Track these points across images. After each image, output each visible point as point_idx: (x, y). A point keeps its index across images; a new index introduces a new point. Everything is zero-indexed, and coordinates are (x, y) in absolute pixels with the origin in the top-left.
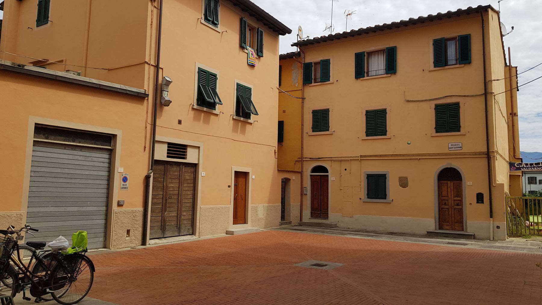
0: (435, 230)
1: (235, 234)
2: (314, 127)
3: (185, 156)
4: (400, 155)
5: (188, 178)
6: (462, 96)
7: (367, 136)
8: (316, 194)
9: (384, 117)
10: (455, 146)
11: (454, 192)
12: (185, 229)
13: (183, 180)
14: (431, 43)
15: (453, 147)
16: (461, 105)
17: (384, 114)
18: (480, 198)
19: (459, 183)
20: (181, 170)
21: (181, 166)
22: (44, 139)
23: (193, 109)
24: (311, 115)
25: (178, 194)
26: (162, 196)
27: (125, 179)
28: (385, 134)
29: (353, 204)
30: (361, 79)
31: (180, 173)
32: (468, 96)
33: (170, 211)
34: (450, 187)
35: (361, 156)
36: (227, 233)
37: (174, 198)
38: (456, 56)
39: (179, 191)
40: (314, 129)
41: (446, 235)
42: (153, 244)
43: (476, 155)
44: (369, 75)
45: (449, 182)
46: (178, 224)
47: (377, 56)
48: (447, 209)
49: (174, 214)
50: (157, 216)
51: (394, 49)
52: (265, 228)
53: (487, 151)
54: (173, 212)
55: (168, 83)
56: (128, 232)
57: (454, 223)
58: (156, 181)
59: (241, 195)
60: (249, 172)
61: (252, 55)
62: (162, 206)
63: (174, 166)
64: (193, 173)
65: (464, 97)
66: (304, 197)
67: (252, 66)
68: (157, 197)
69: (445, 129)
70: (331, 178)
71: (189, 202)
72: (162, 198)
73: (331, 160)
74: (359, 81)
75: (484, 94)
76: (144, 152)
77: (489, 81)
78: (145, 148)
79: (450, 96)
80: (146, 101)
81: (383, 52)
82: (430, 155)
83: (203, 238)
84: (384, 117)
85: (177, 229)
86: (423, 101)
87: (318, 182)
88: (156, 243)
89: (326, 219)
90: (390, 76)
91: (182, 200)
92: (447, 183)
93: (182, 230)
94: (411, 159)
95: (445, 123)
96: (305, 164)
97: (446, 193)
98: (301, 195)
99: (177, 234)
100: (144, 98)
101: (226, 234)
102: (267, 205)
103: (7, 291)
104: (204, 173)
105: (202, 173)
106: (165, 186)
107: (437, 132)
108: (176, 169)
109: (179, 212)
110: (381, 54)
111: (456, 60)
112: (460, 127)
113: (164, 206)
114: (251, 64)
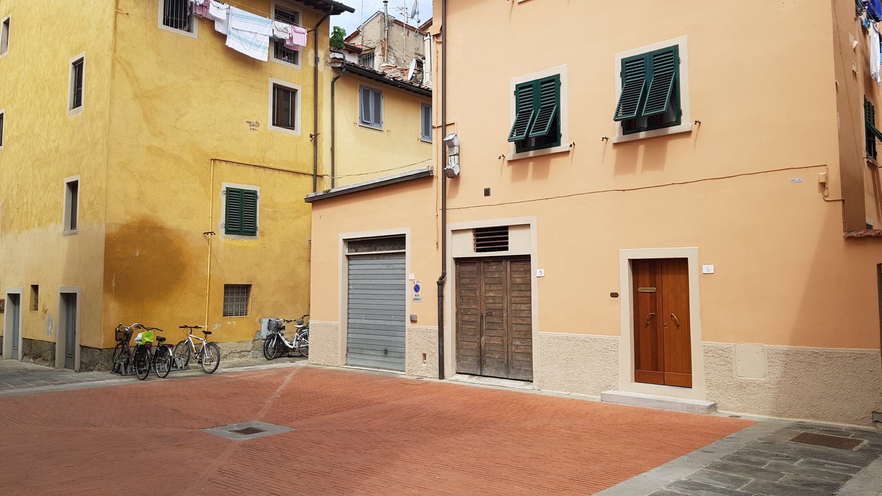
22: (354, 252)
27: (417, 289)
33: (492, 335)
52: (772, 414)
54: (496, 338)
56: (425, 355)
58: (466, 289)
63: (492, 264)
68: (469, 313)
71: (525, 323)
83: (547, 392)
99: (503, 375)
102: (785, 347)
103: (805, 428)
104: (542, 270)
106: (479, 296)
108: (497, 268)
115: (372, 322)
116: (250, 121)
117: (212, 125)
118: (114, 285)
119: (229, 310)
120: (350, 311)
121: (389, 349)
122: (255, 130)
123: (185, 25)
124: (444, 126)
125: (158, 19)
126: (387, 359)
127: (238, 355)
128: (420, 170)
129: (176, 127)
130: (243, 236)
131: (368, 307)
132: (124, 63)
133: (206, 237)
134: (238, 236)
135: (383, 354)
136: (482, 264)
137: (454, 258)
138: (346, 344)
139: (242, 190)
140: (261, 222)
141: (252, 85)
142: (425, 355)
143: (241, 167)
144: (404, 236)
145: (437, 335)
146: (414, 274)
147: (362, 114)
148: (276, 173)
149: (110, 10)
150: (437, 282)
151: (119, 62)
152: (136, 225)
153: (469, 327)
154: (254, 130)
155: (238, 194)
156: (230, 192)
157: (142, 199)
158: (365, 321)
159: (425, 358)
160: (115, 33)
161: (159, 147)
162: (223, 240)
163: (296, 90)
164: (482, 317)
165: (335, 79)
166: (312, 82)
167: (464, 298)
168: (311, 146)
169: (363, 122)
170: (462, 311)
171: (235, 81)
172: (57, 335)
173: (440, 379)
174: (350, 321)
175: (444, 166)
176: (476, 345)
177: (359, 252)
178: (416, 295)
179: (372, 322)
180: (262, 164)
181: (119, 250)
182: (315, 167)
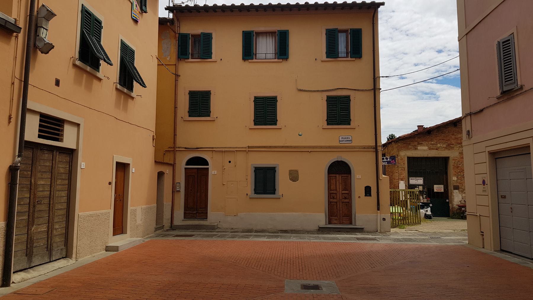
0: (326, 225)
1: (120, 250)
2: (191, 111)
3: (59, 136)
4: (291, 147)
5: (62, 170)
6: (353, 90)
7: (255, 124)
8: (191, 190)
9: (274, 105)
10: (345, 140)
11: (342, 185)
12: (57, 250)
13: (56, 175)
14: (324, 32)
15: (343, 140)
16: (351, 98)
17: (275, 102)
18: (368, 191)
19: (347, 176)
20: (54, 160)
21: (54, 153)
23: (75, 65)
24: (187, 97)
25: (49, 196)
26: (28, 201)
28: (276, 124)
29: (237, 200)
30: (250, 61)
31: (52, 163)
32: (358, 90)
33: (39, 223)
34: (338, 181)
35: (249, 147)
36: (108, 249)
37: (45, 203)
38: (347, 49)
39: (50, 191)
40: (191, 113)
41: (339, 230)
42: (19, 282)
43: (365, 148)
44: (257, 58)
45: (337, 175)
46: (49, 243)
47: (265, 39)
48: (335, 203)
49: (44, 228)
50: (21, 233)
51: (286, 33)
53: (375, 145)
54: (43, 225)
55: (51, 15)
57: (342, 216)
59: (119, 195)
60: (130, 164)
61: (136, 7)
62: (29, 216)
64: (69, 163)
65: (354, 91)
66: (176, 195)
67: (136, 21)
69: (336, 121)
70: (212, 172)
72: (28, 203)
73: (212, 150)
74: (247, 62)
75: (373, 89)
76: (8, 125)
77: (377, 77)
78: (10, 118)
79: (341, 88)
80: (13, 38)
81: (272, 34)
82: (321, 147)
84: (274, 105)
85: (48, 252)
86: (314, 91)
87: (194, 176)
88: (23, 278)
89: (205, 219)
90: (282, 62)
91: (54, 205)
92: (336, 176)
93: (54, 253)
94: (301, 151)
95: (336, 115)
96: (178, 154)
97: (335, 186)
98: (173, 192)
100: (13, 32)
101: (106, 251)
102: (144, 206)
104: (84, 163)
105: (82, 164)
107: (328, 124)
109: (50, 224)
110: (270, 35)
111: (347, 53)
112: (350, 120)
113: (31, 217)
114: (135, 18)
172: (498, 58)
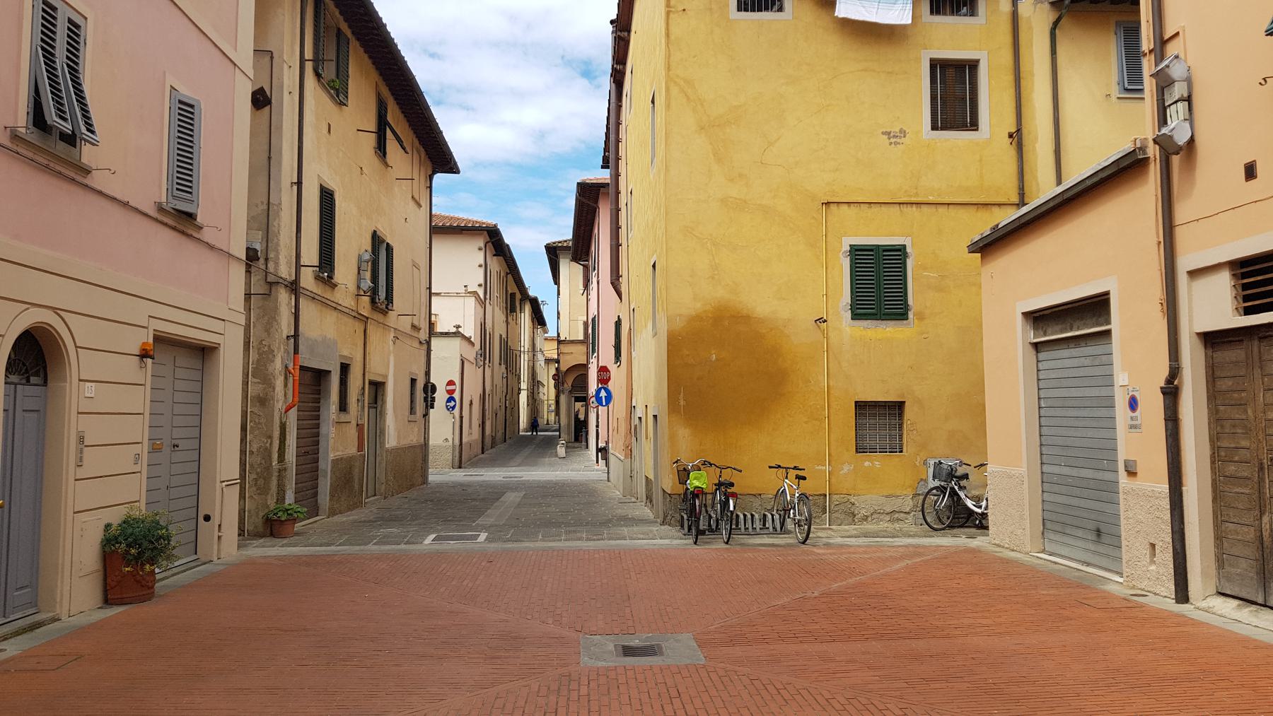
22: (1042, 337)
56: (1153, 546)
58: (1227, 402)
68: (1236, 458)
115: (1074, 472)
116: (888, 130)
117: (822, 149)
118: (682, 403)
119: (868, 443)
120: (1045, 450)
121: (1103, 528)
122: (899, 143)
123: (773, 4)
124: (1162, 43)
125: (728, 5)
126: (1101, 549)
127: (888, 518)
128: (1122, 151)
129: (763, 162)
130: (885, 322)
131: (1069, 442)
132: (682, 83)
133: (819, 326)
134: (875, 322)
135: (1094, 538)
136: (1256, 343)
137: (1198, 334)
138: (1041, 512)
139: (879, 246)
140: (913, 297)
141: (890, 70)
142: (1153, 546)
143: (875, 209)
144: (1106, 297)
145: (1166, 504)
146: (1126, 375)
147: (1123, 71)
148: (942, 210)
149: (662, 10)
150: (1161, 388)
151: (675, 82)
152: (710, 315)
153: (1237, 490)
154: (896, 143)
155: (872, 253)
156: (857, 253)
157: (716, 277)
158: (1066, 471)
159: (1153, 554)
160: (668, 43)
161: (738, 197)
162: (848, 329)
163: (978, 61)
164: (1261, 468)
165: (1055, 24)
166: (1007, 39)
167: (1224, 423)
168: (1011, 152)
169: (1127, 90)
170: (1223, 454)
171: (858, 71)
173: (1178, 602)
174: (1046, 468)
175: (1162, 122)
176: (1251, 534)
177: (1049, 335)
178: (1132, 418)
179: (1074, 472)
180: (913, 199)
181: (687, 353)
182: (1020, 189)
